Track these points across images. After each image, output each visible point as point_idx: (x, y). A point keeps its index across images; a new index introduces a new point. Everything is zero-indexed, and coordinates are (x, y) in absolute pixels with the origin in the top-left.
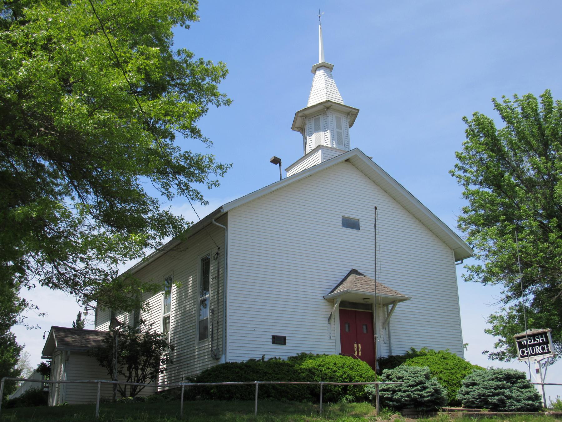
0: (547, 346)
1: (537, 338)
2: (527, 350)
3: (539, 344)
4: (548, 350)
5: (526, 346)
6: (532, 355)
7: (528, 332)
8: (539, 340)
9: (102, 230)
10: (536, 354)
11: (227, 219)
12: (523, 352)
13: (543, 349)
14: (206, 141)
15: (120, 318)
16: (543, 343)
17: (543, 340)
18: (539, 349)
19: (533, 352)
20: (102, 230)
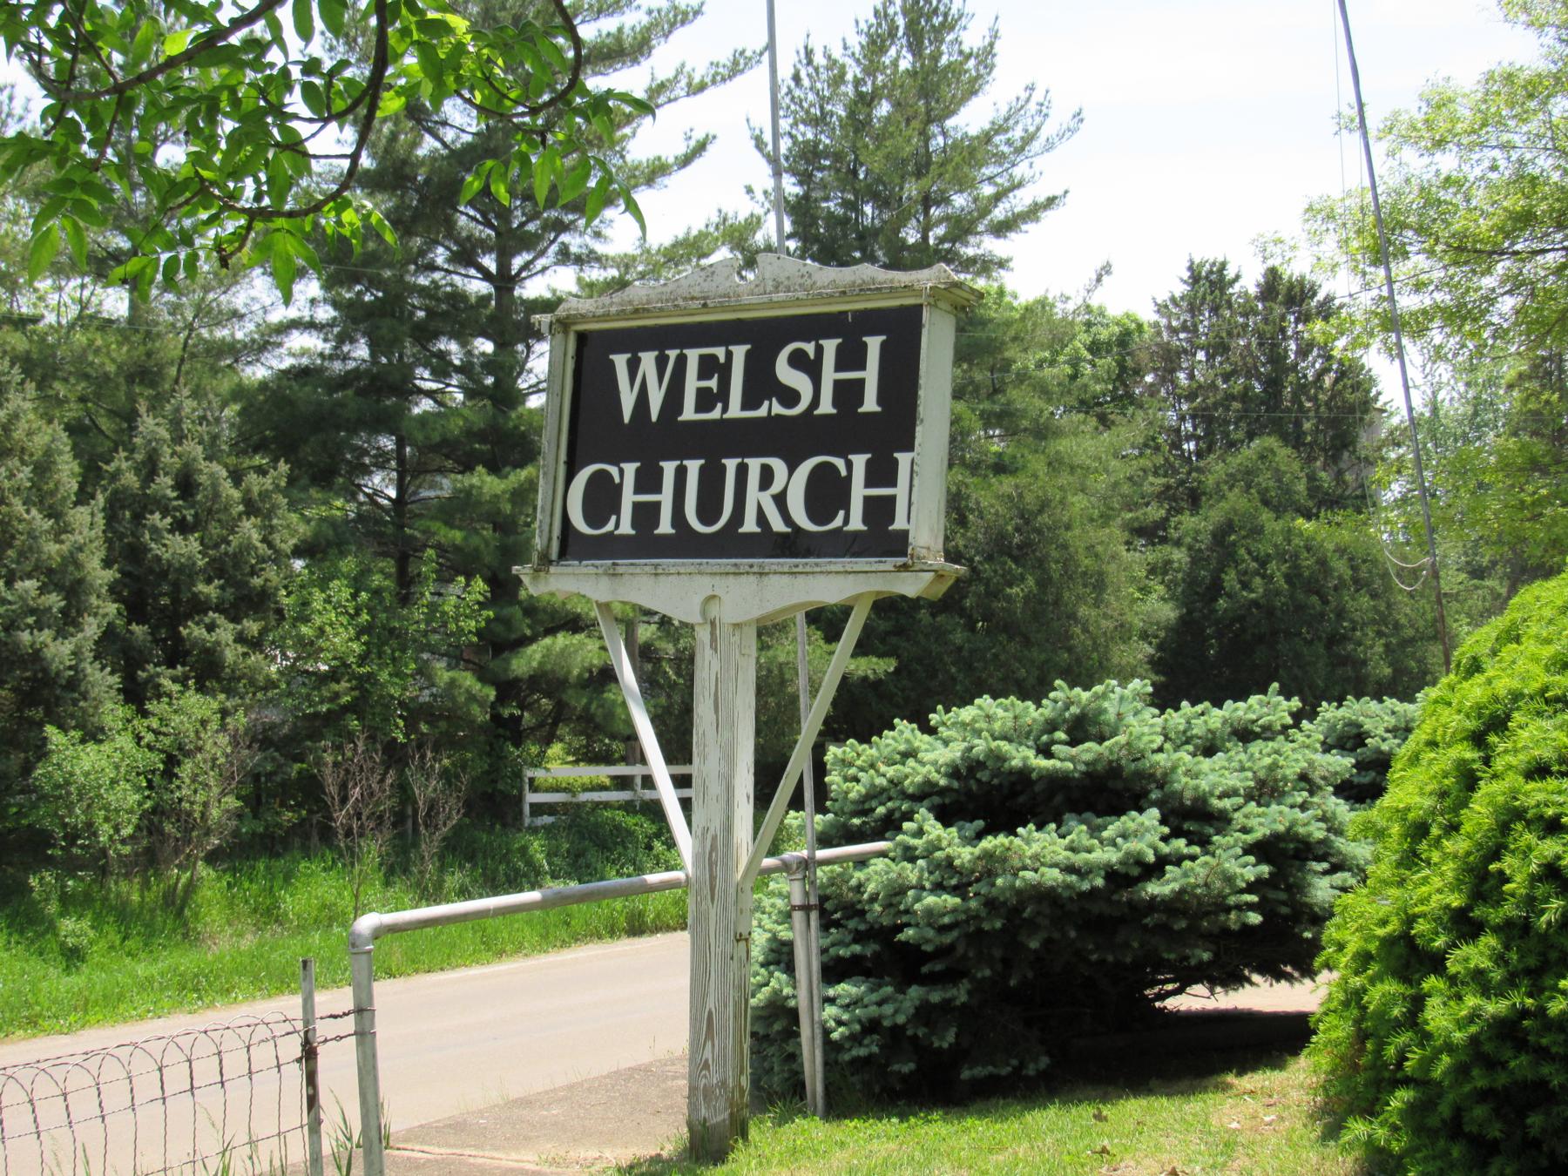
0: (882, 473)
1: (798, 360)
2: (649, 481)
3: (790, 439)
4: (880, 510)
5: (656, 440)
6: (685, 544)
7: (472, 213)
8: (809, 390)
9: (78, 811)
10: (731, 544)
11: (756, 774)
12: (602, 499)
13: (827, 493)
14: (995, 36)
15: (27, 12)
16: (845, 429)
17: (848, 393)
18: (775, 491)
19: (709, 511)
20: (78, 811)
